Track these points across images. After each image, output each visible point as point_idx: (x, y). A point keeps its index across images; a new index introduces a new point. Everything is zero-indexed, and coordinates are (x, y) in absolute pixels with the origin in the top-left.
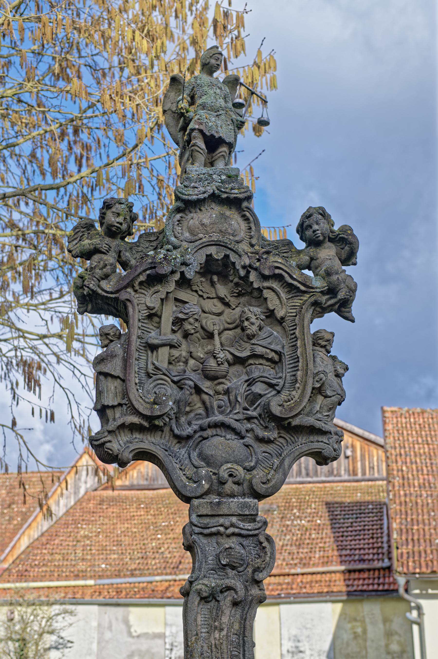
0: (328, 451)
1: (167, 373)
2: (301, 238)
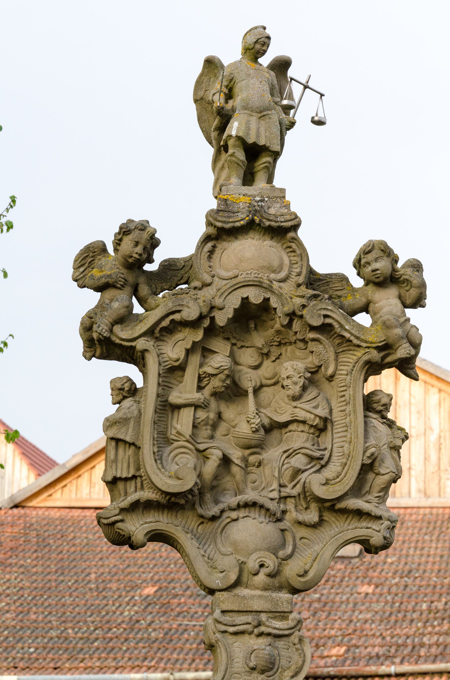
0: (377, 540)
1: (191, 440)
2: (359, 274)
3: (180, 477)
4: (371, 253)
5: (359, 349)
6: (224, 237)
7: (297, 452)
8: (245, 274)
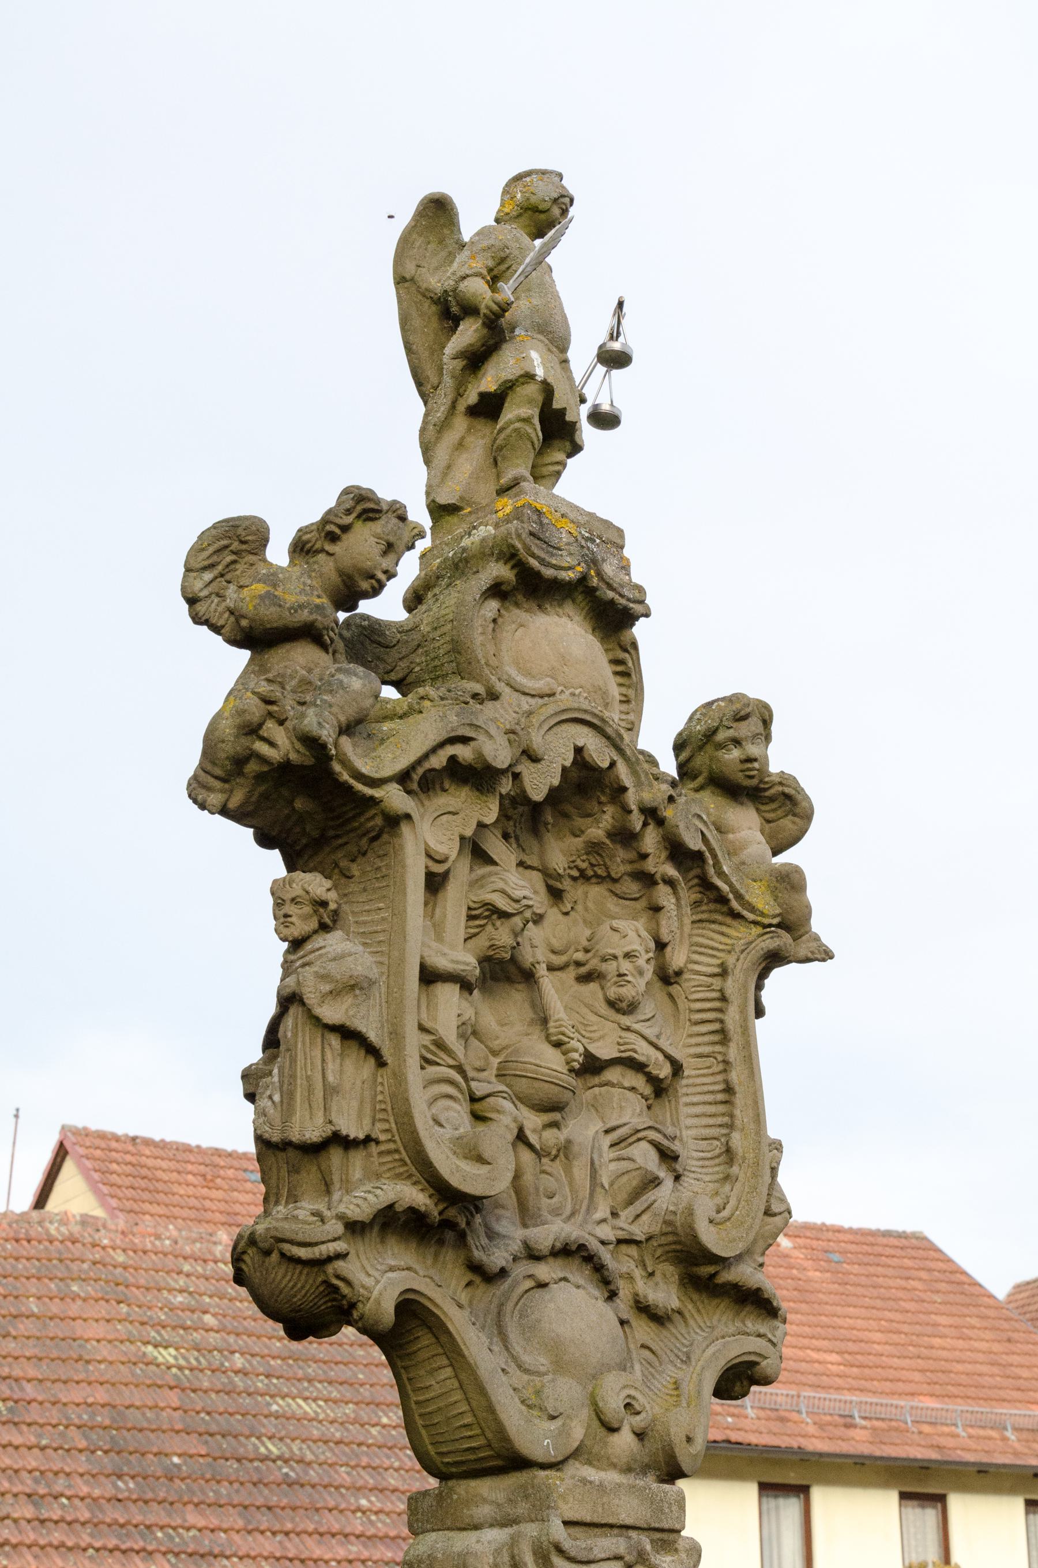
3: (486, 1155)
4: (746, 722)
5: (735, 923)
6: (520, 597)
7: (640, 1135)
8: (567, 693)
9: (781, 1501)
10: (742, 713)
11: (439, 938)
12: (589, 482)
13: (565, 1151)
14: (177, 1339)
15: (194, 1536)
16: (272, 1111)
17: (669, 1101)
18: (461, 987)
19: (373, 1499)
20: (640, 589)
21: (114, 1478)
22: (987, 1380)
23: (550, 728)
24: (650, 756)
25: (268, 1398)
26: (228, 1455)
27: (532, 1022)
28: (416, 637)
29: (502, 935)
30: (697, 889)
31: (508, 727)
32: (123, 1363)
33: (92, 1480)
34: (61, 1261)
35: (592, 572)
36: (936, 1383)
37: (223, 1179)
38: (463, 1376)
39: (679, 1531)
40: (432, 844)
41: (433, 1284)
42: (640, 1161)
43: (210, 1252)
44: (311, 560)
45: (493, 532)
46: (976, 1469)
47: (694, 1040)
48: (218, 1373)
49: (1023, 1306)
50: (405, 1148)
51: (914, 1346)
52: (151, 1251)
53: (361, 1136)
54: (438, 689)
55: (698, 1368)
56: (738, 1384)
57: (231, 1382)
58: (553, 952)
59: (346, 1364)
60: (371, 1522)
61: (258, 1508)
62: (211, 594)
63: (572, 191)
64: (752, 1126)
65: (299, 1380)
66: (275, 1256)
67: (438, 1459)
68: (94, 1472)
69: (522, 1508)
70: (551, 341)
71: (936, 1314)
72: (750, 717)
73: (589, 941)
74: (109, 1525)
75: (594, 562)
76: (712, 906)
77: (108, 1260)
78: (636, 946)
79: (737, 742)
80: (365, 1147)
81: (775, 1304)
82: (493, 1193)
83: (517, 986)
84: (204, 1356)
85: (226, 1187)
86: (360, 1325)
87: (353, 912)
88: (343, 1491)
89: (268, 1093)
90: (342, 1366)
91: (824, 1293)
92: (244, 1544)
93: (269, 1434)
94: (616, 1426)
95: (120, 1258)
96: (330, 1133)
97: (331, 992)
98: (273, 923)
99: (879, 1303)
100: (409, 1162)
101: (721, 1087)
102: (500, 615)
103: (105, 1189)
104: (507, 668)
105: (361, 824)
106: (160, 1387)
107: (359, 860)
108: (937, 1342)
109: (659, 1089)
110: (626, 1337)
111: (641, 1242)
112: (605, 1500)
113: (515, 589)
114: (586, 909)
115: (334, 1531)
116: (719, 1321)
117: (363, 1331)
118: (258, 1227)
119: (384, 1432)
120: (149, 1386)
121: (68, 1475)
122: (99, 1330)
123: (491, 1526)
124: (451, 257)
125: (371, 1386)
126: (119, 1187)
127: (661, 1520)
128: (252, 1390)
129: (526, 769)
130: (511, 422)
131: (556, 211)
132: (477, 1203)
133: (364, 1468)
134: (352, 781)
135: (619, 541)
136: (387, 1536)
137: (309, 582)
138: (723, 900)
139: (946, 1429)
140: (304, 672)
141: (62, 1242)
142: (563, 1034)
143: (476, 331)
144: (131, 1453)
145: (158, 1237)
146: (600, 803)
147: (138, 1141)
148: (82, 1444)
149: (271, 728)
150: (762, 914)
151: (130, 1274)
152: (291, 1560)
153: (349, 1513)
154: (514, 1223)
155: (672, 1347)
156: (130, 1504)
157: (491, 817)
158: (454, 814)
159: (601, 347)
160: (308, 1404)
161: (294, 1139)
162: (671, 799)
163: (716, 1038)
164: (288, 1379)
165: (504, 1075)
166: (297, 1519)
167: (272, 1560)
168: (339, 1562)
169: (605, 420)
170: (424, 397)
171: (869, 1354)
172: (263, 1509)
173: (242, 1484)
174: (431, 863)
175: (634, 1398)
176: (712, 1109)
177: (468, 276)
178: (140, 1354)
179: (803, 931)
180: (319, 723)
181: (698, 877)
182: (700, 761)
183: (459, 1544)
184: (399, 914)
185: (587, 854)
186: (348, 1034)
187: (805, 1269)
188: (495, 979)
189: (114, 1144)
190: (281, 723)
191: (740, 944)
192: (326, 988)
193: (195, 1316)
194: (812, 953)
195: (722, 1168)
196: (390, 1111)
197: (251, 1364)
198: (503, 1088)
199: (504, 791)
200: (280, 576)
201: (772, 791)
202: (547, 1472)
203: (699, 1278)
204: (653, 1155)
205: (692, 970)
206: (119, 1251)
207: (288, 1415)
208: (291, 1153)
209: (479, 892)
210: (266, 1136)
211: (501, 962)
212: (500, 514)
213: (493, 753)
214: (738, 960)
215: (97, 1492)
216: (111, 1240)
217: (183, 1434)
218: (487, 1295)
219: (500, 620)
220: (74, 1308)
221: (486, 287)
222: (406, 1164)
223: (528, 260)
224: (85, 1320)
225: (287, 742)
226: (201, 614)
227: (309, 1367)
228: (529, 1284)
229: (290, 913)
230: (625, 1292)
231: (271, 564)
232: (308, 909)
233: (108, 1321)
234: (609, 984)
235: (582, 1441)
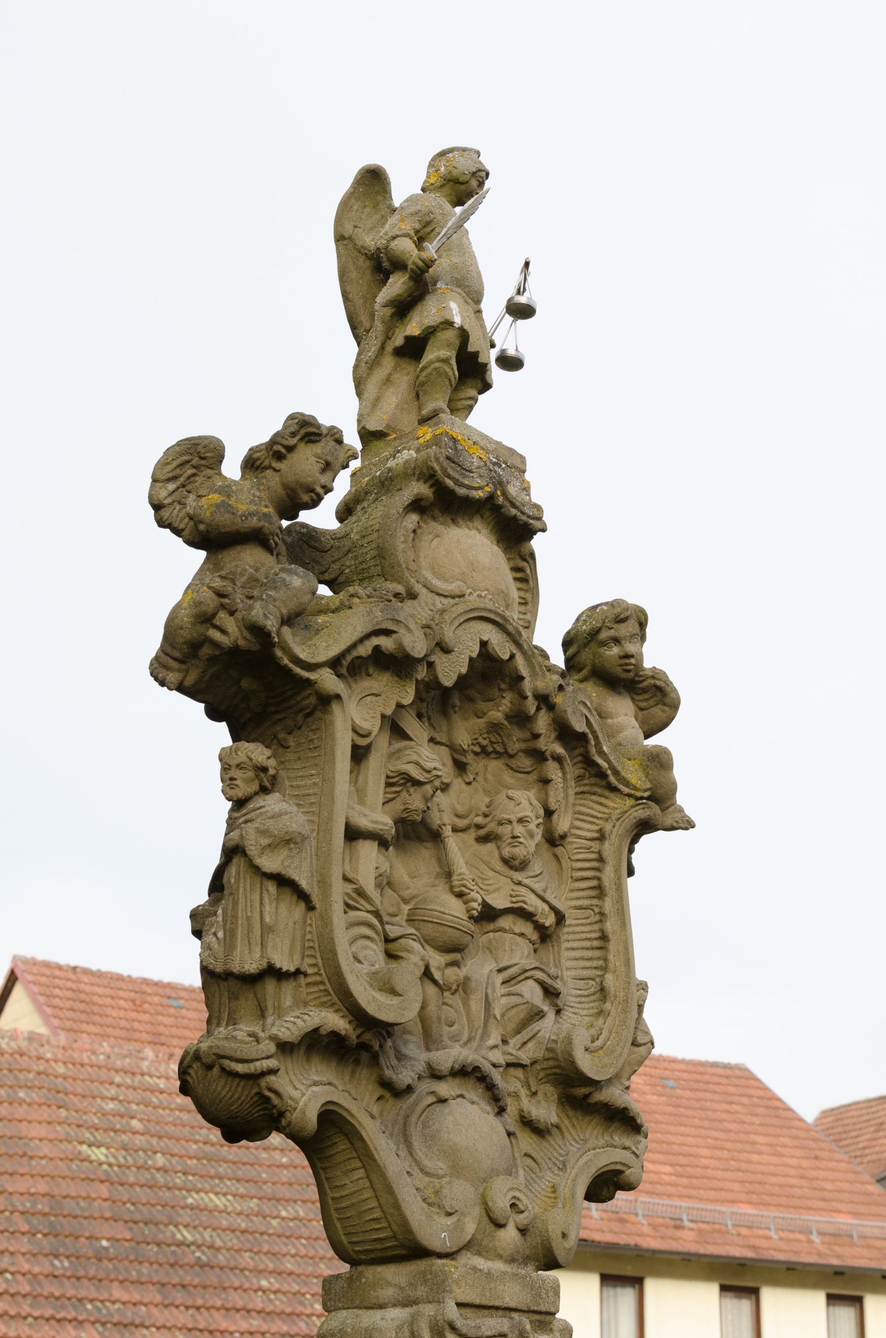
3: (399, 988)
4: (626, 624)
5: (612, 795)
6: (436, 512)
7: (528, 974)
8: (475, 594)
9: (619, 1290)
10: (622, 616)
11: (362, 801)
12: (496, 415)
13: (464, 986)
14: (108, 1140)
15: (119, 1309)
16: (216, 946)
17: (553, 946)
18: (379, 844)
19: (272, 1280)
20: (538, 508)
21: (51, 1257)
22: (797, 1192)
23: (460, 624)
24: (542, 651)
25: (184, 1192)
26: (149, 1240)
27: (438, 876)
28: (347, 543)
29: (415, 800)
30: (580, 765)
31: (424, 622)
32: (61, 1159)
33: (32, 1259)
34: (10, 1071)
35: (499, 492)
36: (753, 1193)
37: (150, 1004)
38: (374, 1177)
39: (554, 1314)
40: (358, 721)
41: (350, 1098)
42: (527, 996)
43: (138, 1066)
44: (260, 475)
45: (415, 455)
46: (785, 1267)
47: (574, 895)
48: (142, 1170)
49: (828, 1129)
50: (329, 981)
51: (735, 1160)
52: (88, 1065)
53: (292, 969)
54: (365, 588)
55: (572, 1175)
56: (605, 1190)
57: (153, 1178)
58: (457, 816)
59: (252, 1165)
60: (271, 1301)
61: (174, 1286)
62: (173, 502)
63: (488, 166)
64: (623, 969)
65: (211, 1177)
66: (216, 1071)
67: (350, 1248)
68: (35, 1251)
69: (421, 1291)
70: (468, 294)
71: (754, 1134)
72: (628, 620)
73: (488, 807)
74: (47, 1298)
75: (500, 484)
76: (593, 780)
77: (50, 1071)
78: (528, 813)
79: (617, 641)
80: (295, 979)
81: (639, 1121)
82: (403, 1021)
83: (425, 844)
84: (130, 1155)
85: (152, 1011)
86: (287, 1130)
87: (288, 778)
88: (247, 1273)
89: (213, 930)
90: (248, 1167)
91: (660, 1114)
92: (161, 1316)
93: (185, 1223)
94: (503, 1222)
95: (61, 1069)
96: (265, 965)
97: (270, 845)
98: (220, 785)
99: (706, 1123)
100: (332, 992)
101: (597, 935)
102: (419, 527)
103: (49, 1011)
104: (424, 572)
105: (298, 703)
106: (92, 1180)
107: (294, 733)
108: (755, 1157)
109: (545, 935)
110: (512, 1147)
111: (526, 1066)
112: (492, 1285)
113: (432, 504)
114: (486, 780)
115: (238, 1307)
116: (591, 1135)
117: (290, 1136)
118: (202, 1045)
119: (283, 1223)
120: (83, 1180)
121: (12, 1254)
122: (41, 1131)
123: (394, 1306)
124: (383, 220)
125: (273, 1184)
126: (61, 1009)
127: (539, 1304)
128: (171, 1185)
129: (438, 659)
130: (431, 362)
131: (474, 183)
132: (389, 1029)
133: (265, 1254)
134: (291, 665)
135: (521, 466)
136: (283, 1312)
137: (258, 494)
138: (602, 775)
139: (760, 1232)
140: (252, 571)
141: (11, 1055)
142: (465, 886)
143: (403, 283)
144: (66, 1237)
145: (94, 1052)
146: (500, 690)
147: (78, 970)
148: (25, 1227)
149: (223, 618)
150: (635, 788)
151: (70, 1083)
152: (201, 1331)
153: (251, 1292)
154: (419, 1047)
155: (551, 1156)
156: (65, 1281)
157: (408, 700)
158: (377, 695)
159: (509, 300)
160: (219, 1199)
161: (234, 971)
162: (561, 688)
163: (593, 893)
164: (202, 1177)
165: (414, 920)
166: (207, 1296)
167: (184, 1331)
168: (242, 1334)
169: (511, 363)
170: (357, 337)
171: (697, 1166)
172: (178, 1287)
173: (161, 1265)
174: (356, 737)
175: (518, 1199)
176: (590, 954)
177: (398, 236)
178: (76, 1152)
179: (669, 803)
180: (265, 615)
181: (581, 755)
182: (586, 656)
183: (367, 1320)
184: (329, 779)
185: (488, 733)
186: (283, 882)
187: (644, 1093)
188: (407, 837)
189: (57, 973)
190: (232, 613)
191: (616, 814)
192: (265, 841)
193: (124, 1121)
194: (677, 822)
195: (597, 1004)
196: (317, 949)
197: (170, 1163)
198: (413, 931)
199: (419, 677)
200: (234, 488)
201: (645, 684)
202: (443, 1261)
203: (575, 1097)
204: (538, 991)
205: (575, 835)
206: (60, 1064)
207: (202, 1207)
208: (232, 983)
209: (396, 763)
210: (211, 967)
211: (414, 823)
212: (421, 440)
213: (411, 645)
214: (614, 827)
215: (36, 1269)
216: (53, 1054)
217: (112, 1222)
218: (394, 1108)
219: (419, 531)
220: (21, 1112)
221: (413, 246)
222: (330, 995)
223: (450, 224)
224: (30, 1122)
225: (236, 630)
226: (165, 518)
227: (220, 1166)
228: (431, 1099)
229: (236, 777)
230: (512, 1108)
231: (226, 478)
232: (250, 774)
233: (49, 1123)
234: (504, 845)
235: (473, 1235)
